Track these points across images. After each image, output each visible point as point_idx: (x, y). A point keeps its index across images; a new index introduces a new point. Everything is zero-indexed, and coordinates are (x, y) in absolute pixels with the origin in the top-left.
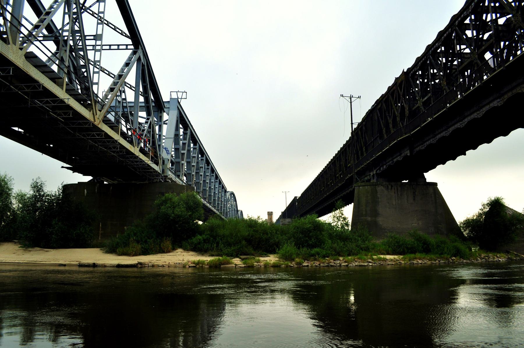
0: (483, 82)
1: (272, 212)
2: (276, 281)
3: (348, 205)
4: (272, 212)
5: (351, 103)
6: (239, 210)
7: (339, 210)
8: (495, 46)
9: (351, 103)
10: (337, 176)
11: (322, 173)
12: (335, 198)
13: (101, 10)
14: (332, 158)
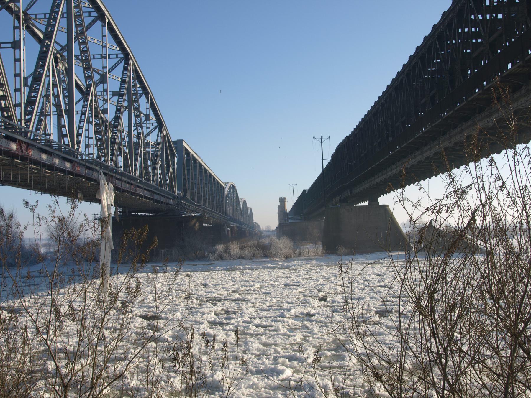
0: (526, 59)
1: (285, 198)
2: (403, 367)
3: (409, 185)
4: (285, 198)
5: (322, 143)
6: (242, 199)
7: (464, 166)
8: (484, 58)
9: (322, 143)
10: (374, 145)
11: (390, 91)
12: (393, 171)
13: (43, 16)
14: (394, 76)
